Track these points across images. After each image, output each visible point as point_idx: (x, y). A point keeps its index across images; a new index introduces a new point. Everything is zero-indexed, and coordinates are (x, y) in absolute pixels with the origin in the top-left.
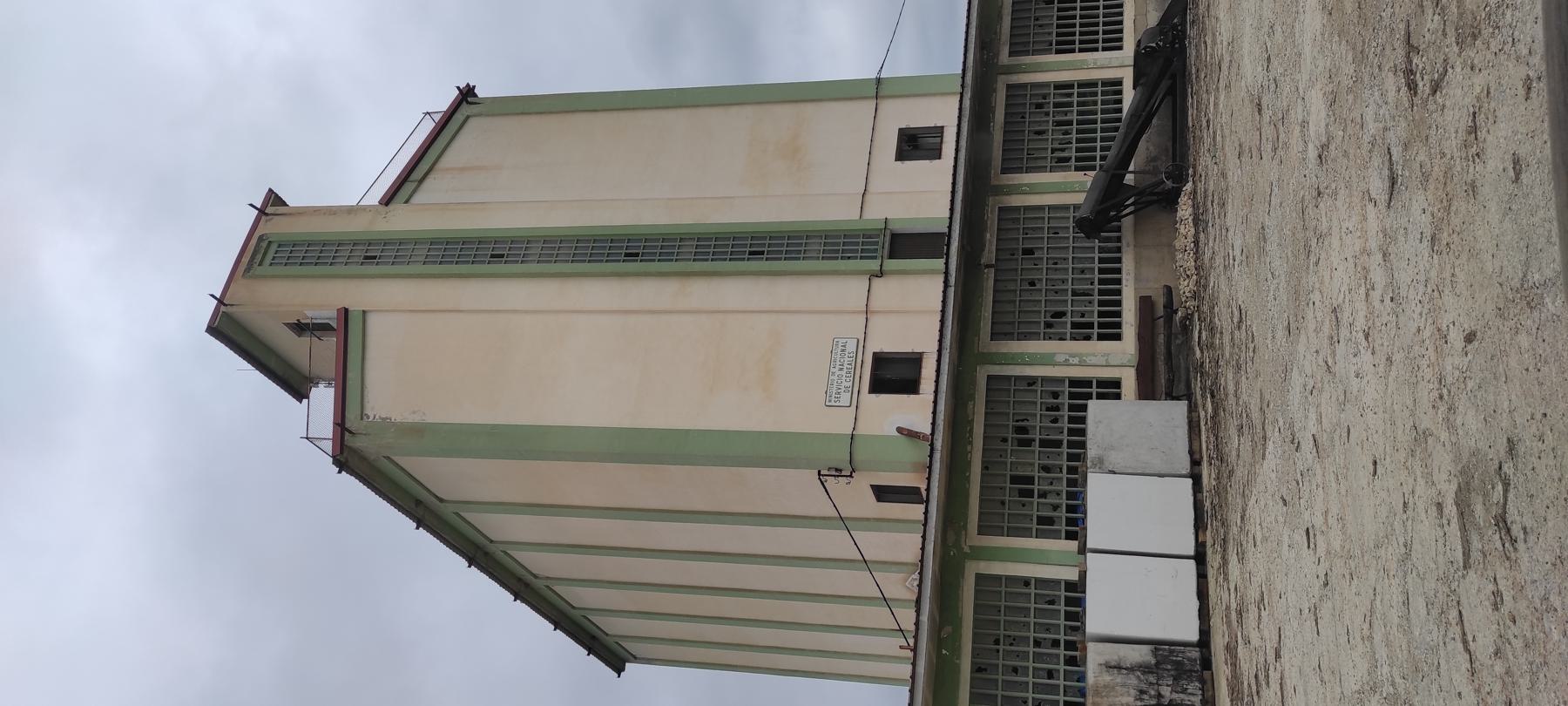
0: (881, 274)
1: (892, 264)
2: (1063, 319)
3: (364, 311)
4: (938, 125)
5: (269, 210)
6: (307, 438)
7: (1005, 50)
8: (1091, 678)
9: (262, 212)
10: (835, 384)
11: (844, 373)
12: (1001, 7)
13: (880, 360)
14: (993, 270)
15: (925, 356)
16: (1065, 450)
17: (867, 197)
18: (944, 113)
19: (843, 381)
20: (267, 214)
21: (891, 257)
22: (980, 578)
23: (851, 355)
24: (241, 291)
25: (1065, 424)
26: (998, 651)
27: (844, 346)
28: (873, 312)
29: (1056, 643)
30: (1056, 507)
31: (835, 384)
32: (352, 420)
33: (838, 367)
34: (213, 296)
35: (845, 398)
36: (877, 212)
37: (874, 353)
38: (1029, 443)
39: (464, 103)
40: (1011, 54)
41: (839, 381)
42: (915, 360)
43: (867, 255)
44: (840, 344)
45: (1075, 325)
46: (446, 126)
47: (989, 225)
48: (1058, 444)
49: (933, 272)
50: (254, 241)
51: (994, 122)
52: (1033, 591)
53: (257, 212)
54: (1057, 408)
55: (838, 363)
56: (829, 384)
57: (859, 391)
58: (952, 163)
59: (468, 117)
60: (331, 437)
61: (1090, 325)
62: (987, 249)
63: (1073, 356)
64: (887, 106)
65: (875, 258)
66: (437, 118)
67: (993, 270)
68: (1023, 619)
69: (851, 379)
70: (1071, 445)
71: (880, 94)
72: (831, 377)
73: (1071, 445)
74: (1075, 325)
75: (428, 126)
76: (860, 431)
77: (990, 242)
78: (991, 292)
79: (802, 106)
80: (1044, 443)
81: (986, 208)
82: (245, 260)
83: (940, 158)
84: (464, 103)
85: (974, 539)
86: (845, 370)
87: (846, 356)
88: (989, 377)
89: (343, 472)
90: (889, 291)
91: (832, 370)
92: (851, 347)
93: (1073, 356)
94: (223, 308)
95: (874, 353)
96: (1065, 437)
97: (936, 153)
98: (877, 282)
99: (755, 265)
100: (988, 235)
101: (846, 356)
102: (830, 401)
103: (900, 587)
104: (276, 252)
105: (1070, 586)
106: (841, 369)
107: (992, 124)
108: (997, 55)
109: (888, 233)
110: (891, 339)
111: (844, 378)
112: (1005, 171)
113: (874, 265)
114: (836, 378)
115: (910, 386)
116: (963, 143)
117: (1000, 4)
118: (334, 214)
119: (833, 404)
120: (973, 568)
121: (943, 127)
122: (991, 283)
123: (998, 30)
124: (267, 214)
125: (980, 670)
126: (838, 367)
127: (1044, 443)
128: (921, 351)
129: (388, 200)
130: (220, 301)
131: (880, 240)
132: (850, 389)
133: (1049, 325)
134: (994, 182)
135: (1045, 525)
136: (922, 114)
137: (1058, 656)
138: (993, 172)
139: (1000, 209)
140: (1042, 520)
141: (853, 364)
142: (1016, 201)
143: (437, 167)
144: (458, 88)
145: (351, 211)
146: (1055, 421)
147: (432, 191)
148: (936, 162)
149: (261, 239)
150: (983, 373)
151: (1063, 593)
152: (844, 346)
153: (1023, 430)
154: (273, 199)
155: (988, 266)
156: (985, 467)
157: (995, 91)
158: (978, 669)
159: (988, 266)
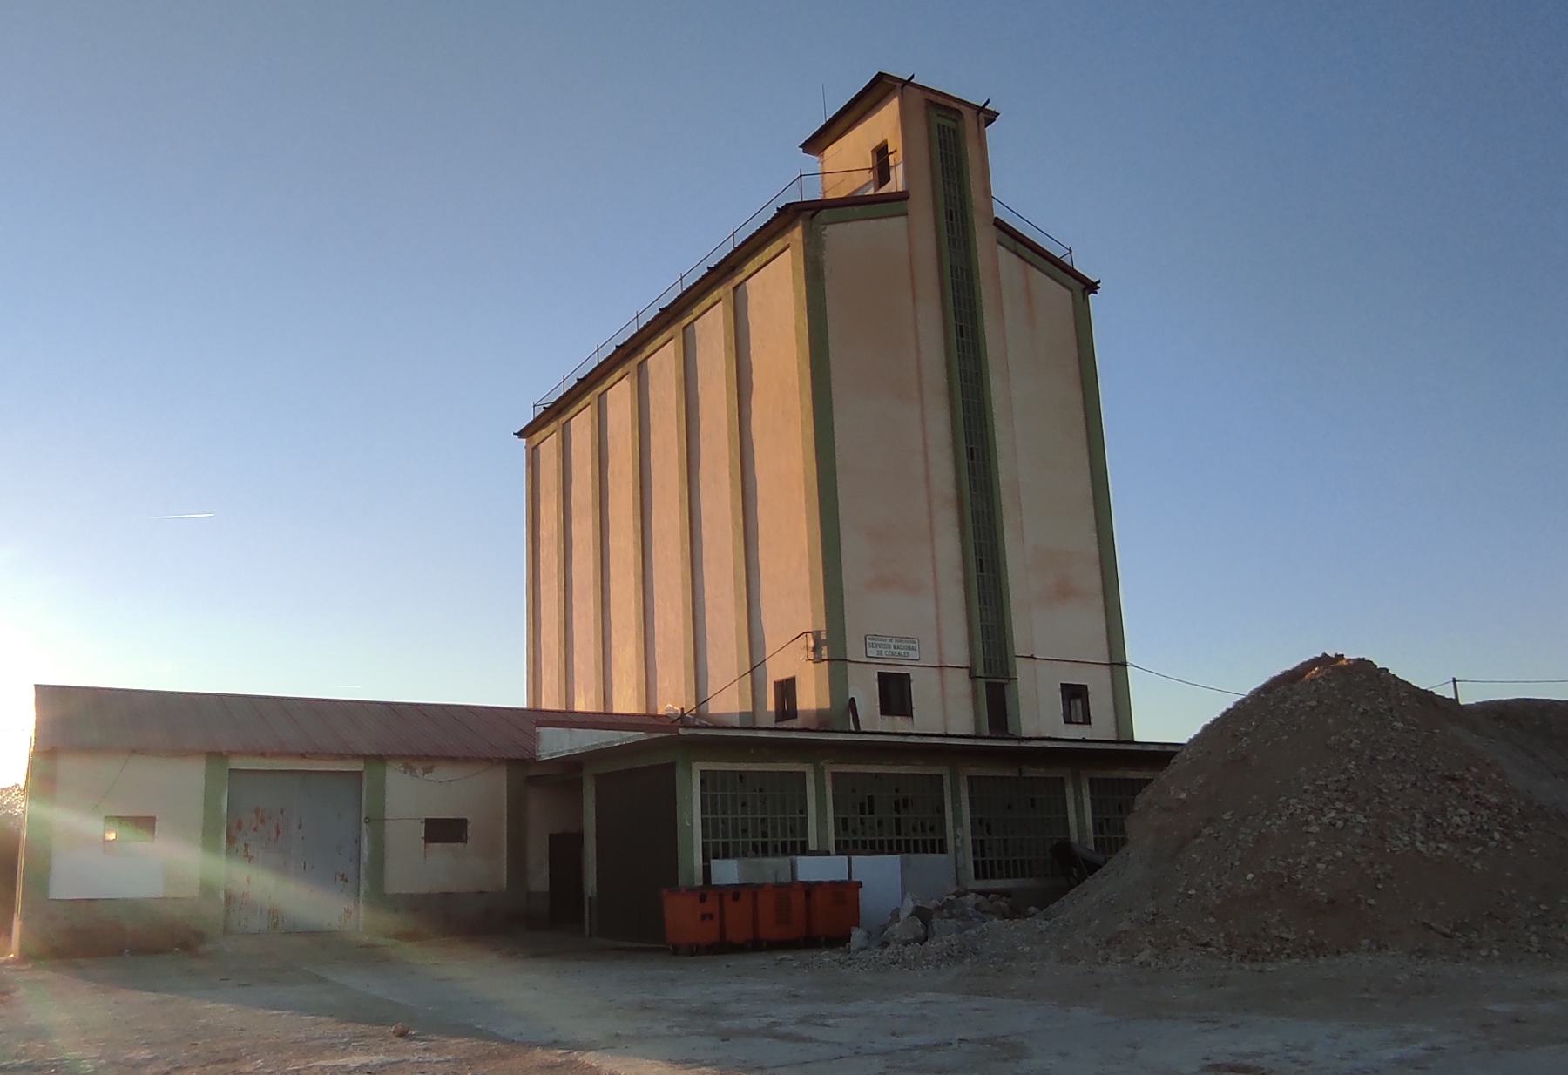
0: (973, 677)
1: (982, 684)
2: (986, 834)
3: (907, 214)
4: (914, 711)
5: (982, 115)
6: (801, 176)
8: (768, 861)
9: (982, 109)
11: (892, 650)
13: (905, 679)
14: (1017, 775)
16: (895, 837)
17: (1031, 660)
18: (1100, 728)
20: (978, 114)
21: (988, 684)
22: (802, 776)
25: (913, 837)
26: (755, 791)
28: (942, 675)
29: (765, 835)
30: (855, 832)
32: (824, 214)
33: (896, 644)
34: (988, 102)
36: (1022, 669)
37: (1085, 687)
38: (898, 811)
39: (1083, 286)
40: (969, 778)
42: (906, 711)
43: (988, 665)
45: (982, 842)
46: (1061, 269)
48: (899, 833)
49: (977, 721)
50: (955, 105)
52: (799, 815)
54: (923, 831)
56: (882, 638)
59: (1071, 290)
61: (983, 856)
63: (962, 841)
64: (1105, 673)
65: (985, 672)
66: (1067, 260)
67: (1017, 775)
68: (709, 810)
70: (784, 844)
73: (765, 844)
74: (982, 842)
75: (1057, 252)
78: (1001, 774)
79: (1101, 597)
80: (898, 821)
82: (940, 100)
83: (1065, 722)
84: (1083, 286)
85: (830, 768)
88: (941, 776)
90: (959, 683)
92: (913, 654)
93: (962, 841)
94: (900, 85)
95: (1085, 687)
96: (903, 838)
97: (1068, 720)
98: (966, 672)
99: (973, 565)
103: (672, 699)
104: (949, 128)
105: (804, 844)
106: (895, 648)
110: (923, 689)
111: (888, 650)
112: (1091, 781)
113: (980, 671)
114: (888, 642)
115: (886, 709)
119: (868, 641)
120: (808, 769)
121: (1090, 723)
122: (1008, 774)
124: (978, 114)
125: (741, 777)
126: (896, 644)
127: (898, 821)
129: (999, 224)
130: (908, 83)
133: (981, 822)
135: (842, 824)
136: (1100, 702)
137: (757, 837)
139: (1062, 778)
140: (845, 821)
142: (1070, 791)
143: (1029, 267)
144: (1099, 282)
145: (987, 190)
146: (914, 829)
147: (1008, 262)
149: (959, 112)
150: (943, 770)
151: (798, 839)
153: (905, 806)
154: (991, 117)
155: (1020, 770)
156: (877, 775)
158: (742, 776)
159: (1020, 770)
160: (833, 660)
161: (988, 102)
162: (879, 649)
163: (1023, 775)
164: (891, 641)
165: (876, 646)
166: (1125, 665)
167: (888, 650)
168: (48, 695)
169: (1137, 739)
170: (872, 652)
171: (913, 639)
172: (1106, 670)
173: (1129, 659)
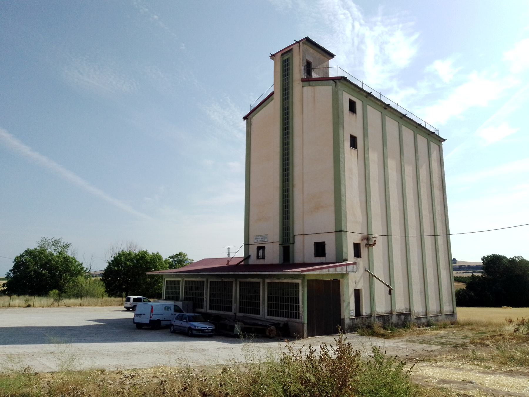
40: (268, 283)
100: (228, 279)
112: (240, 283)
149: (291, 50)
159: (222, 280)
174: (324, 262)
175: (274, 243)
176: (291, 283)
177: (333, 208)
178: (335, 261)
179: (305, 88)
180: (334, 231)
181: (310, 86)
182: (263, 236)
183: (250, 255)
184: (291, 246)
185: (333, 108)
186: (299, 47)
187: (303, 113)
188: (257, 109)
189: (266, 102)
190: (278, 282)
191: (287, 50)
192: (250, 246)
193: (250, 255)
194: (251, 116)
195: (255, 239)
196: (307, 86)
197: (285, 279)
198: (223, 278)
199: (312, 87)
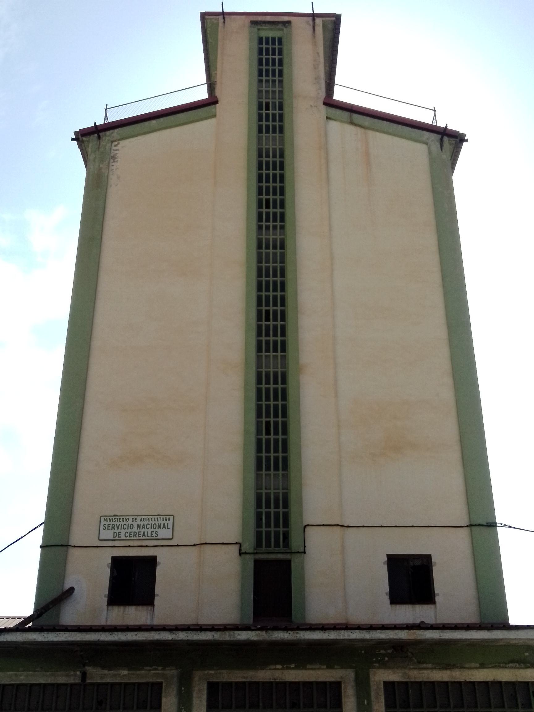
7: (394, 676)
10: (123, 523)
11: (135, 529)
12: (462, 667)
14: (78, 680)
15: (150, 608)
19: (126, 530)
23: (154, 535)
24: (233, 24)
27: (164, 527)
31: (123, 523)
34: (107, 105)
35: (108, 534)
40: (389, 686)
41: (125, 526)
44: (166, 523)
47: (138, 672)
50: (286, 19)
51: (283, 668)
53: (222, 11)
55: (146, 523)
56: (123, 517)
57: (114, 546)
58: (387, 621)
60: (109, 122)
62: (106, 672)
69: (128, 538)
71: (474, 528)
72: (130, 518)
75: (426, 118)
76: (72, 550)
77: (115, 676)
81: (160, 668)
86: (137, 531)
87: (153, 530)
89: (466, 139)
91: (139, 518)
92: (163, 533)
100: (125, 672)
101: (153, 530)
102: (105, 520)
107: (279, 667)
108: (384, 665)
109: (288, 556)
112: (213, 688)
114: (130, 522)
116: (182, 636)
117: (467, 665)
118: (315, 68)
119: (102, 523)
122: (62, 680)
123: (425, 665)
126: (142, 523)
128: (156, 603)
131: (282, 549)
132: (117, 538)
134: (197, 675)
138: (213, 672)
141: (144, 538)
148: (387, 599)
149: (289, 22)
152: (164, 527)
157: (330, 667)
159: (84, 675)
160: (47, 546)
161: (107, 105)
162: (117, 531)
163: (88, 681)
164: (135, 520)
165: (113, 528)
166: (492, 525)
167: (129, 530)
168: (466, 134)
169: (513, 620)
170: (108, 534)
171: (166, 517)
172: (464, 534)
173: (499, 518)
174: (430, 620)
175: (207, 548)
176: (513, 684)
177: (455, 455)
178: (473, 619)
179: (332, 124)
180: (465, 522)
181: (352, 123)
182: (148, 517)
183: (72, 589)
184: (295, 561)
185: (247, 230)
186: (314, 27)
187: (328, 179)
188: (147, 123)
189: (172, 118)
190: (446, 679)
191: (268, 18)
192: (74, 555)
193: (72, 589)
194: (116, 133)
195: (107, 528)
196: (341, 121)
197: (483, 666)
198: (89, 669)
199: (359, 130)
